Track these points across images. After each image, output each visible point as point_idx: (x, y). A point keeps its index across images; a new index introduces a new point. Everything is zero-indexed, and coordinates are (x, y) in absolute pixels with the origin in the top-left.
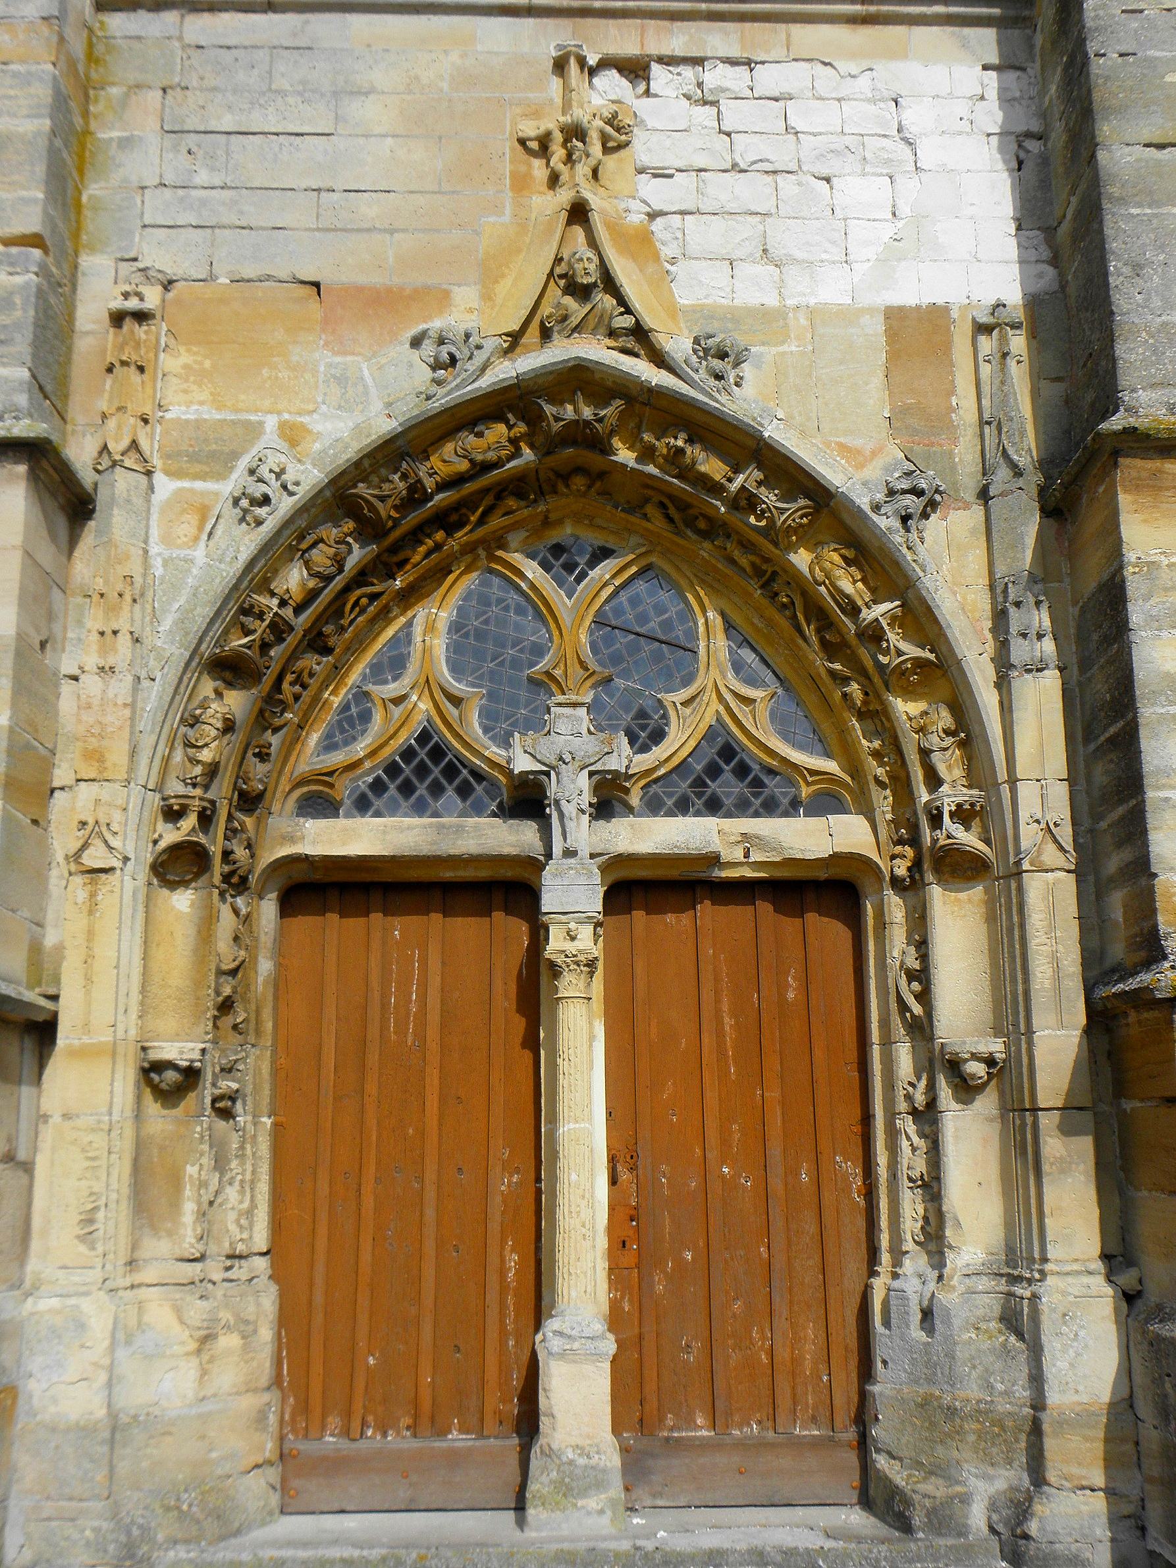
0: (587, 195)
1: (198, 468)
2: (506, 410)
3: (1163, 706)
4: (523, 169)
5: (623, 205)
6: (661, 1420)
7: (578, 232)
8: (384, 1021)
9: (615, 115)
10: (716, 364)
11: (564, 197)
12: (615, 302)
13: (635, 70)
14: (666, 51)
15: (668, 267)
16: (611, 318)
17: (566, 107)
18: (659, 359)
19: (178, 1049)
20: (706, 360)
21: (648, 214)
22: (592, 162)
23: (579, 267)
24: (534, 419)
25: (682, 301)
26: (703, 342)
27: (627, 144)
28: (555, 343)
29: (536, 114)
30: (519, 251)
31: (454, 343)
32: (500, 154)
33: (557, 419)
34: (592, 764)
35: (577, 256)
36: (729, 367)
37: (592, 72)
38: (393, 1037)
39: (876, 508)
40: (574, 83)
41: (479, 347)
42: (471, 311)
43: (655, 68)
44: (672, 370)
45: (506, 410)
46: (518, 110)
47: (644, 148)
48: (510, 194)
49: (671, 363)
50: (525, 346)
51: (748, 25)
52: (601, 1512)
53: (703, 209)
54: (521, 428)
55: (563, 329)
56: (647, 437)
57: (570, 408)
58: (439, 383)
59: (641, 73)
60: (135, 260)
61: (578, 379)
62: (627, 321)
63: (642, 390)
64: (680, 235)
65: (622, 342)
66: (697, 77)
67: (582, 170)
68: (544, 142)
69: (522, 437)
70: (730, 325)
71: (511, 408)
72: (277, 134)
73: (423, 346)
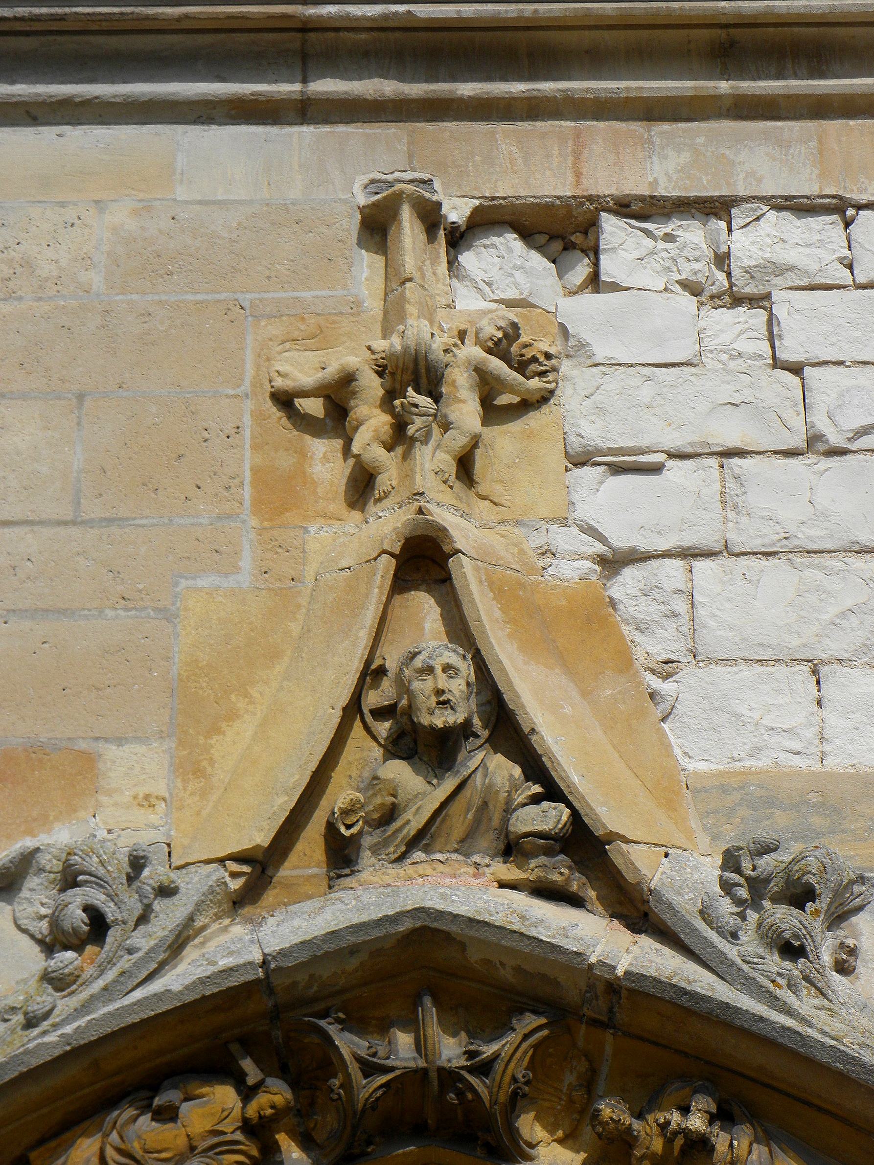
0: (444, 516)
2: (235, 1048)
4: (285, 461)
5: (537, 540)
7: (424, 608)
9: (512, 332)
10: (784, 917)
11: (388, 523)
12: (517, 771)
13: (563, 232)
14: (635, 184)
15: (655, 683)
16: (509, 810)
17: (393, 315)
18: (637, 910)
20: (758, 908)
21: (602, 560)
22: (457, 440)
23: (423, 687)
24: (310, 1071)
25: (692, 766)
26: (746, 865)
27: (545, 398)
28: (365, 876)
29: (319, 338)
30: (275, 655)
31: (100, 882)
32: (229, 429)
33: (370, 1068)
35: (418, 662)
36: (817, 925)
37: (458, 239)
40: (409, 263)
41: (166, 891)
42: (148, 802)
43: (612, 228)
44: (667, 935)
45: (235, 1048)
46: (275, 329)
47: (584, 407)
48: (254, 522)
49: (667, 917)
50: (288, 886)
51: (833, 126)
53: (738, 541)
54: (277, 1094)
55: (386, 842)
56: (610, 1109)
57: (404, 1040)
58: (59, 982)
59: (577, 238)
61: (424, 963)
62: (551, 817)
63: (591, 987)
64: (680, 605)
65: (535, 869)
66: (713, 242)
67: (433, 460)
68: (338, 397)
69: (279, 1113)
70: (817, 821)
71: (248, 1044)
73: (25, 893)
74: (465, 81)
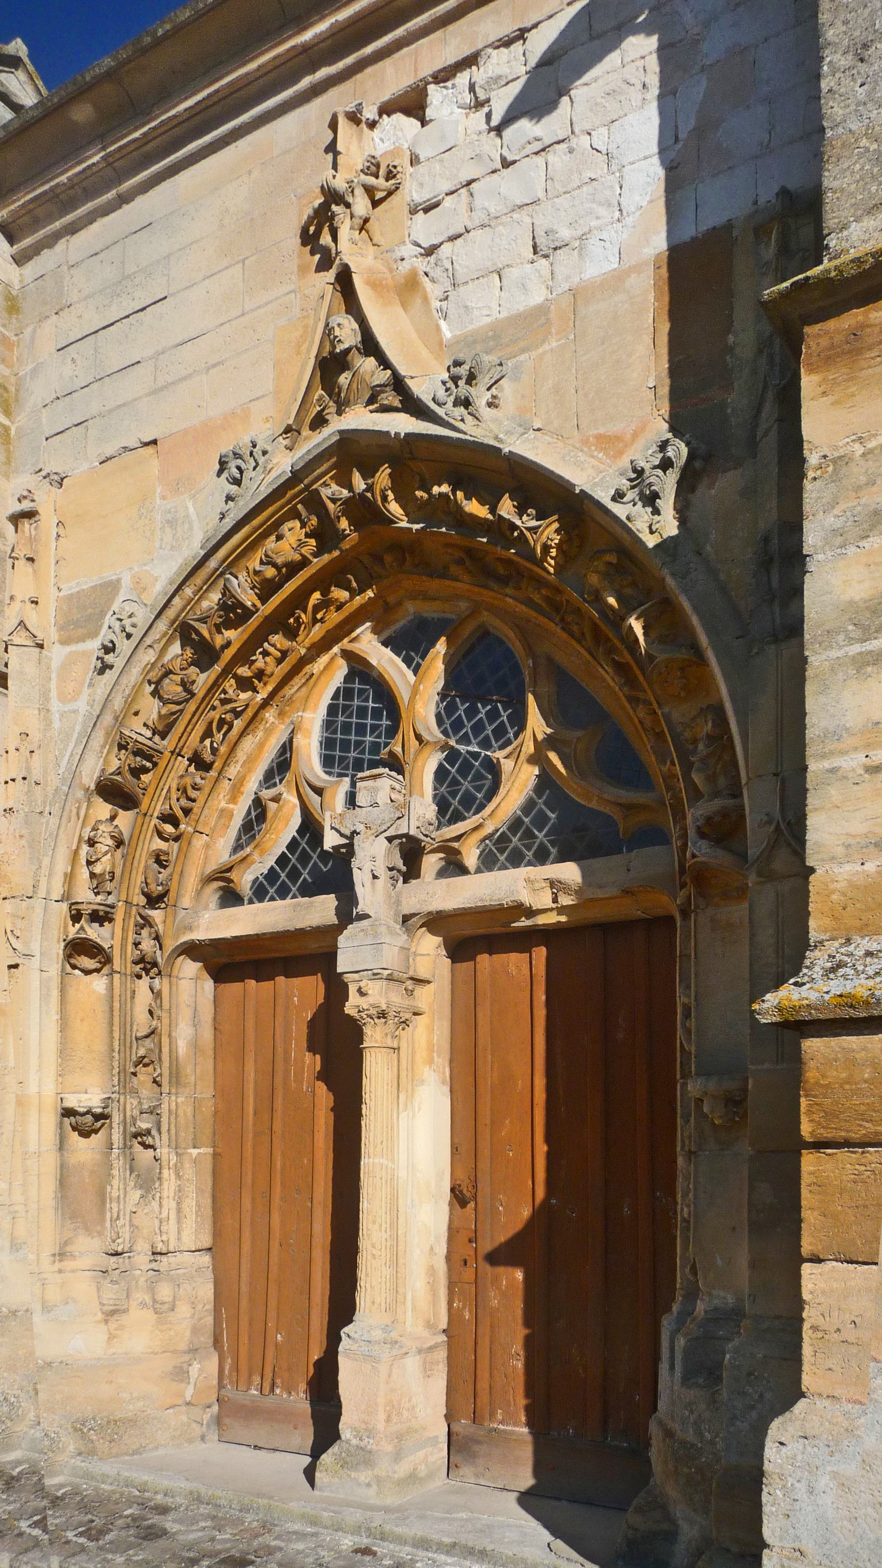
1: (81, 631)
3: (841, 647)
6: (492, 1415)
8: (287, 1072)
18: (413, 406)
19: (89, 1098)
34: (385, 831)
38: (293, 1085)
39: (618, 496)
52: (369, 1485)
60: (40, 470)
72: (127, 317)
74: (366, 46)
